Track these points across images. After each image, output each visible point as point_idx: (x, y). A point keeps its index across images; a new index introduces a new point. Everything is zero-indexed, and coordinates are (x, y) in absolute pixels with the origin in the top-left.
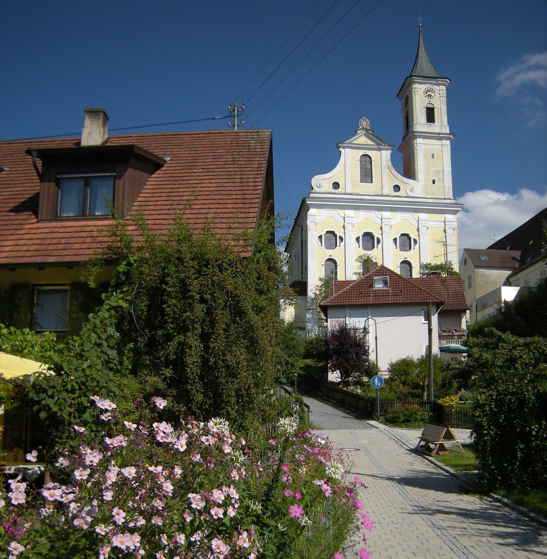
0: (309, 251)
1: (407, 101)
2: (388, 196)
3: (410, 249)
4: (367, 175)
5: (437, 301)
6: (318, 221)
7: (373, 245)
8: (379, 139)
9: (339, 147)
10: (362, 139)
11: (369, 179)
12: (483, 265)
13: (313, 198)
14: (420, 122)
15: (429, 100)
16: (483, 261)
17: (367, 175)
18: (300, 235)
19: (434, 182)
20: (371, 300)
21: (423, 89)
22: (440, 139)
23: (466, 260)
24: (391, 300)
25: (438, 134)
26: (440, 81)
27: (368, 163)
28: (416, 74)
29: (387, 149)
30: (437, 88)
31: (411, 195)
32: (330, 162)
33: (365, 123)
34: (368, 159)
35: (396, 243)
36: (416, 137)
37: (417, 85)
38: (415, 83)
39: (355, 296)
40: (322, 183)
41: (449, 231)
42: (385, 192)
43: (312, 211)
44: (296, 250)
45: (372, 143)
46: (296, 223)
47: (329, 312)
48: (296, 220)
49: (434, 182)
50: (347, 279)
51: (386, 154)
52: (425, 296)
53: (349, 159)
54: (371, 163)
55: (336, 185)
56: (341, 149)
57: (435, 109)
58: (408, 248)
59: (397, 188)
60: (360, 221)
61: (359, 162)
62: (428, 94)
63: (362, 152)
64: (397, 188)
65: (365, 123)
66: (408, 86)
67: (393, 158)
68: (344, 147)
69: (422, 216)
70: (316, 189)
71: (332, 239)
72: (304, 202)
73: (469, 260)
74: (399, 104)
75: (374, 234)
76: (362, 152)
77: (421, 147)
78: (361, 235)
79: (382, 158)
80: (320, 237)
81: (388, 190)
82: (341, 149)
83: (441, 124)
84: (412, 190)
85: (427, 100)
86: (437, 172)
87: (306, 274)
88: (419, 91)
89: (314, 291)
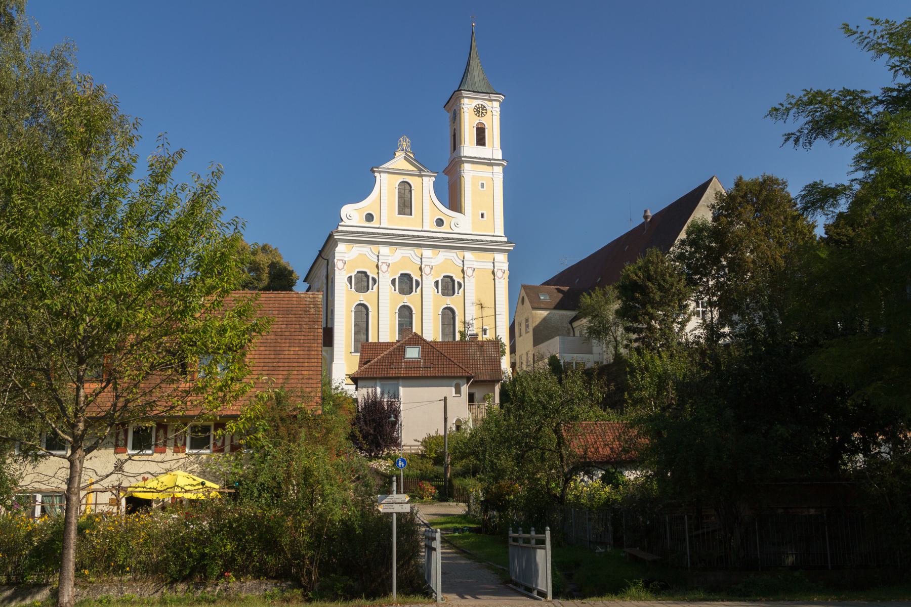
0: (336, 302)
1: (456, 117)
3: (454, 294)
4: (405, 206)
6: (348, 258)
7: (412, 288)
8: (422, 163)
9: (374, 172)
10: (399, 162)
11: (408, 210)
12: (542, 306)
13: (342, 232)
14: (469, 147)
16: (543, 302)
17: (405, 206)
19: (482, 216)
20: (403, 373)
21: (473, 106)
22: (492, 165)
24: (421, 372)
25: (489, 159)
26: (493, 96)
27: (407, 191)
28: (466, 88)
29: (430, 176)
30: (489, 103)
31: (456, 230)
32: (361, 189)
33: (405, 143)
34: (407, 187)
35: (437, 287)
36: (463, 162)
37: (466, 101)
38: (464, 97)
40: (352, 215)
41: (499, 274)
43: (341, 248)
44: (320, 282)
45: (411, 168)
47: (360, 383)
48: (321, 252)
49: (482, 216)
50: (380, 341)
51: (429, 182)
53: (386, 186)
54: (411, 191)
55: (369, 217)
56: (376, 174)
57: (486, 131)
58: (451, 292)
59: (440, 222)
60: (397, 260)
61: (397, 191)
62: (480, 111)
63: (401, 179)
64: (440, 222)
65: (405, 143)
66: (456, 100)
67: (436, 184)
68: (380, 172)
69: (468, 255)
70: (346, 222)
71: (363, 282)
72: (331, 236)
73: (526, 299)
74: (448, 116)
76: (401, 179)
77: (469, 173)
78: (397, 277)
79: (425, 188)
80: (350, 278)
81: (429, 225)
82: (376, 174)
83: (493, 149)
84: (456, 225)
87: (333, 319)
88: (468, 105)
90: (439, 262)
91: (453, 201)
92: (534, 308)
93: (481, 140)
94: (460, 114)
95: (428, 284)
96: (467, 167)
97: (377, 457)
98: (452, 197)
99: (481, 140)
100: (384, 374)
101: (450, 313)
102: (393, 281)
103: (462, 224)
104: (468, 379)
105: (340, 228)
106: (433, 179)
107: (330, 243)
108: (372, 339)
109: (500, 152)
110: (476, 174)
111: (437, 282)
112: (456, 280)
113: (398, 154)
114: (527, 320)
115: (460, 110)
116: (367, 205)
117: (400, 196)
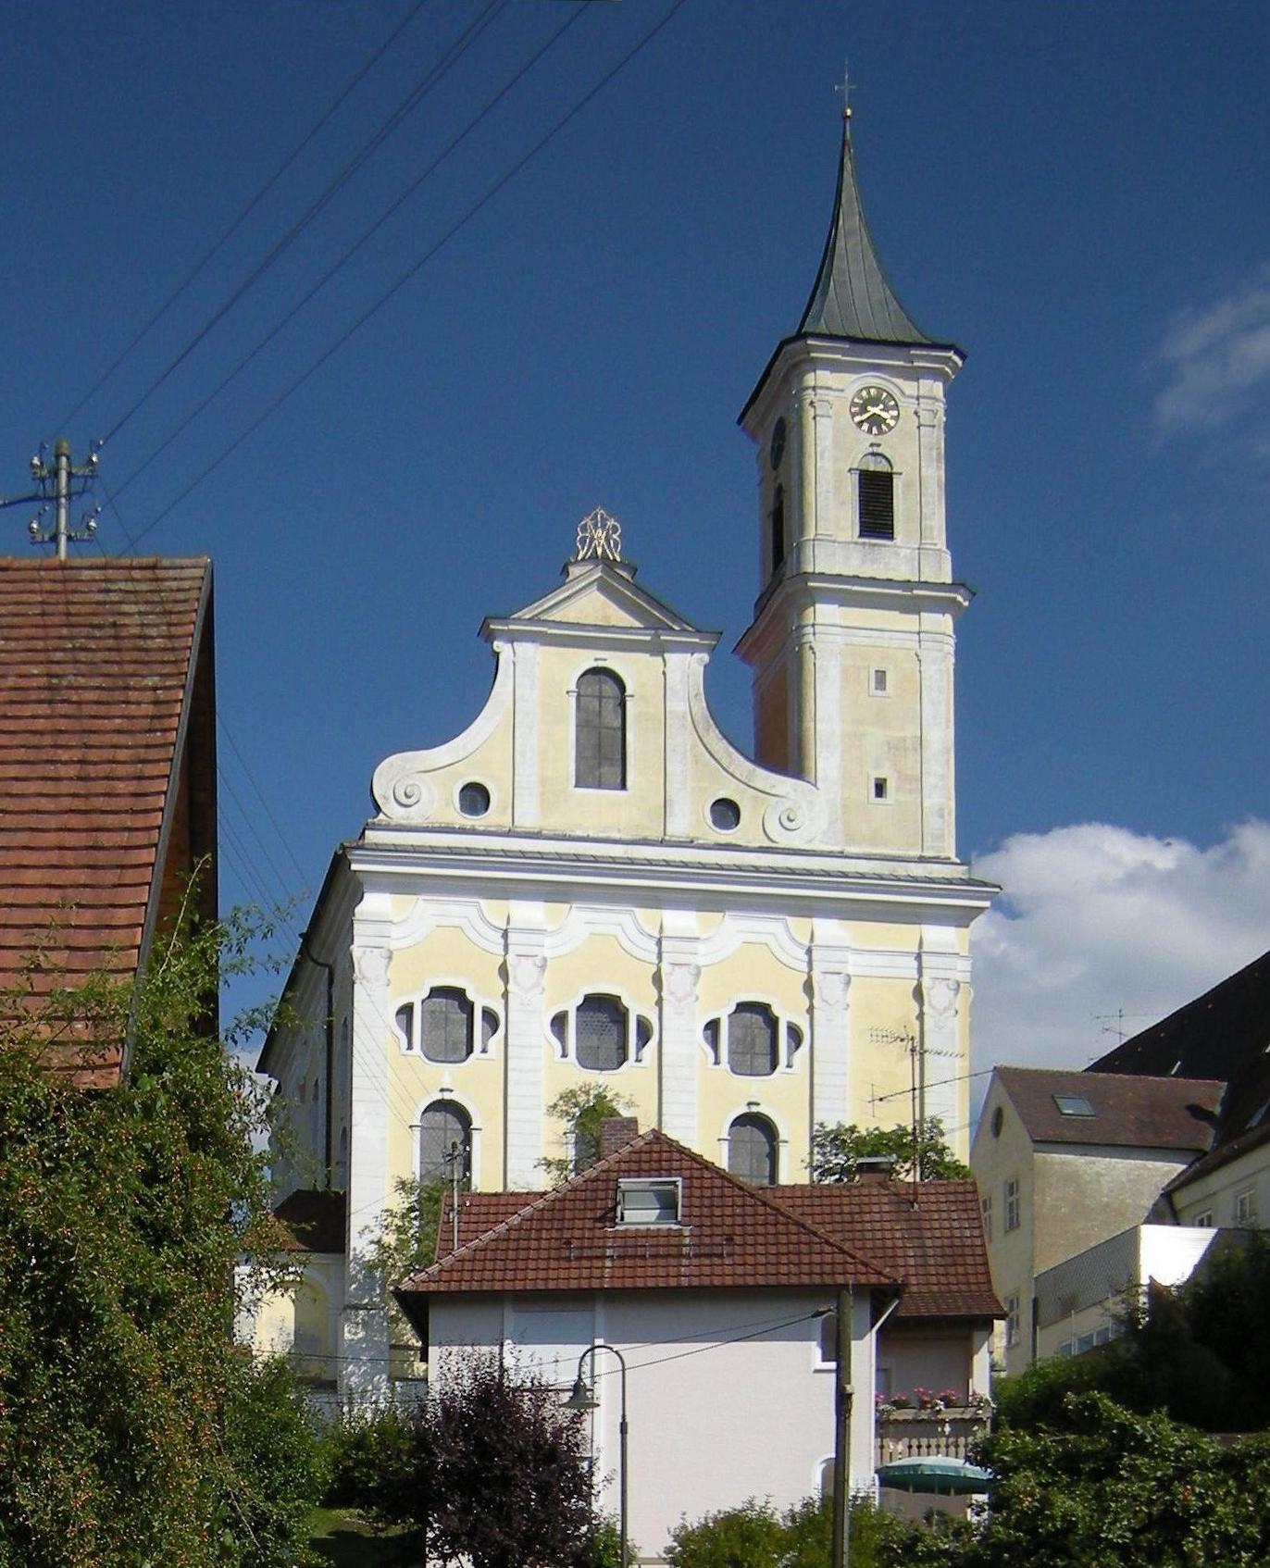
1: (782, 445)
2: (689, 844)
3: (774, 1065)
4: (603, 756)
5: (874, 1279)
6: (400, 944)
8: (660, 606)
10: (587, 604)
15: (872, 439)
17: (603, 756)
18: (323, 1003)
19: (880, 788)
20: (607, 1274)
21: (850, 393)
23: (999, 1114)
24: (686, 1273)
25: (907, 584)
26: (922, 359)
28: (822, 328)
29: (692, 649)
31: (784, 840)
32: (452, 700)
33: (601, 535)
34: (610, 688)
36: (812, 598)
39: (544, 1254)
40: (415, 786)
42: (678, 828)
44: (306, 1063)
45: (621, 618)
46: (305, 951)
47: (437, 1320)
48: (307, 938)
49: (880, 788)
50: (512, 1188)
51: (687, 668)
52: (828, 1258)
53: (534, 684)
54: (623, 705)
55: (476, 797)
56: (497, 645)
57: (897, 481)
58: (766, 1061)
59: (726, 812)
60: (575, 947)
61: (573, 700)
63: (588, 659)
64: (726, 812)
65: (601, 535)
66: (786, 380)
68: (512, 638)
70: (392, 812)
73: (1010, 1114)
74: (747, 454)
75: (626, 1002)
76: (588, 659)
77: (832, 635)
80: (407, 1011)
81: (691, 818)
83: (922, 545)
85: (864, 440)
86: (895, 747)
89: (377, 1233)
90: (731, 956)
91: (775, 737)
92: (1047, 1143)
93: (876, 504)
94: (800, 425)
95: (682, 1037)
96: (824, 615)
97: (873, 561)
98: (769, 726)
99: (876, 504)
100: (533, 1279)
101: (760, 1137)
102: (559, 1022)
103: (803, 816)
104: (879, 1296)
105: (372, 836)
106: (706, 657)
107: (339, 890)
108: (485, 1179)
109: (947, 559)
110: (860, 638)
111: (713, 1026)
112: (784, 1015)
113: (575, 571)
114: (1012, 1188)
115: (800, 412)
116: (473, 751)
117: (586, 723)
